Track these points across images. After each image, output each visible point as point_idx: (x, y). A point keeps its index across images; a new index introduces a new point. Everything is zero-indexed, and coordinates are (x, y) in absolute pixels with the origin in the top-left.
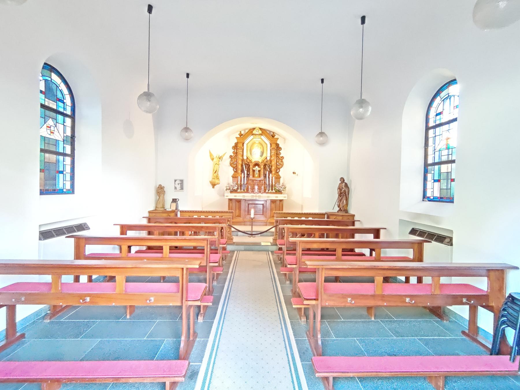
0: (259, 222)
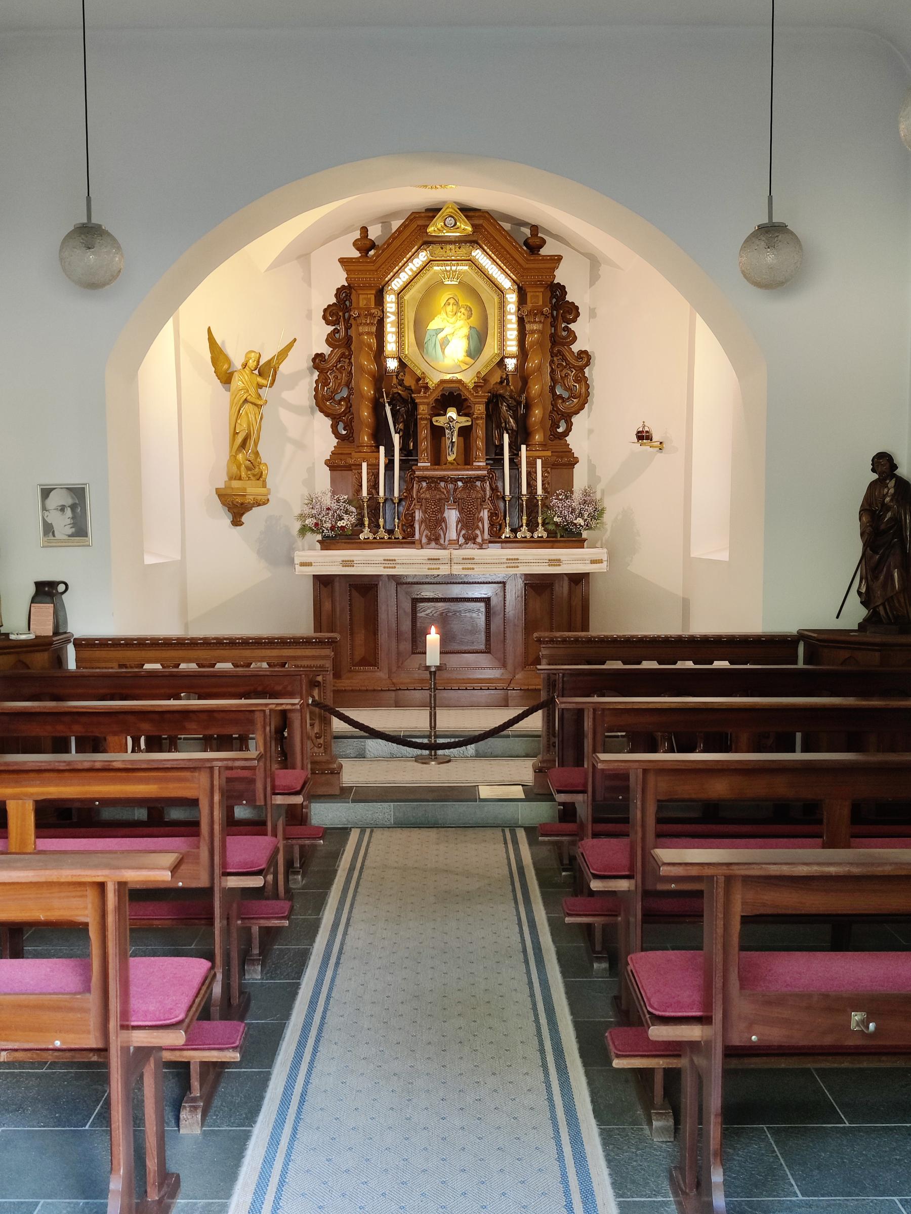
0: (463, 686)
